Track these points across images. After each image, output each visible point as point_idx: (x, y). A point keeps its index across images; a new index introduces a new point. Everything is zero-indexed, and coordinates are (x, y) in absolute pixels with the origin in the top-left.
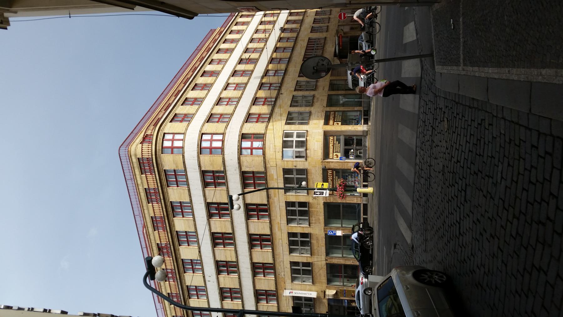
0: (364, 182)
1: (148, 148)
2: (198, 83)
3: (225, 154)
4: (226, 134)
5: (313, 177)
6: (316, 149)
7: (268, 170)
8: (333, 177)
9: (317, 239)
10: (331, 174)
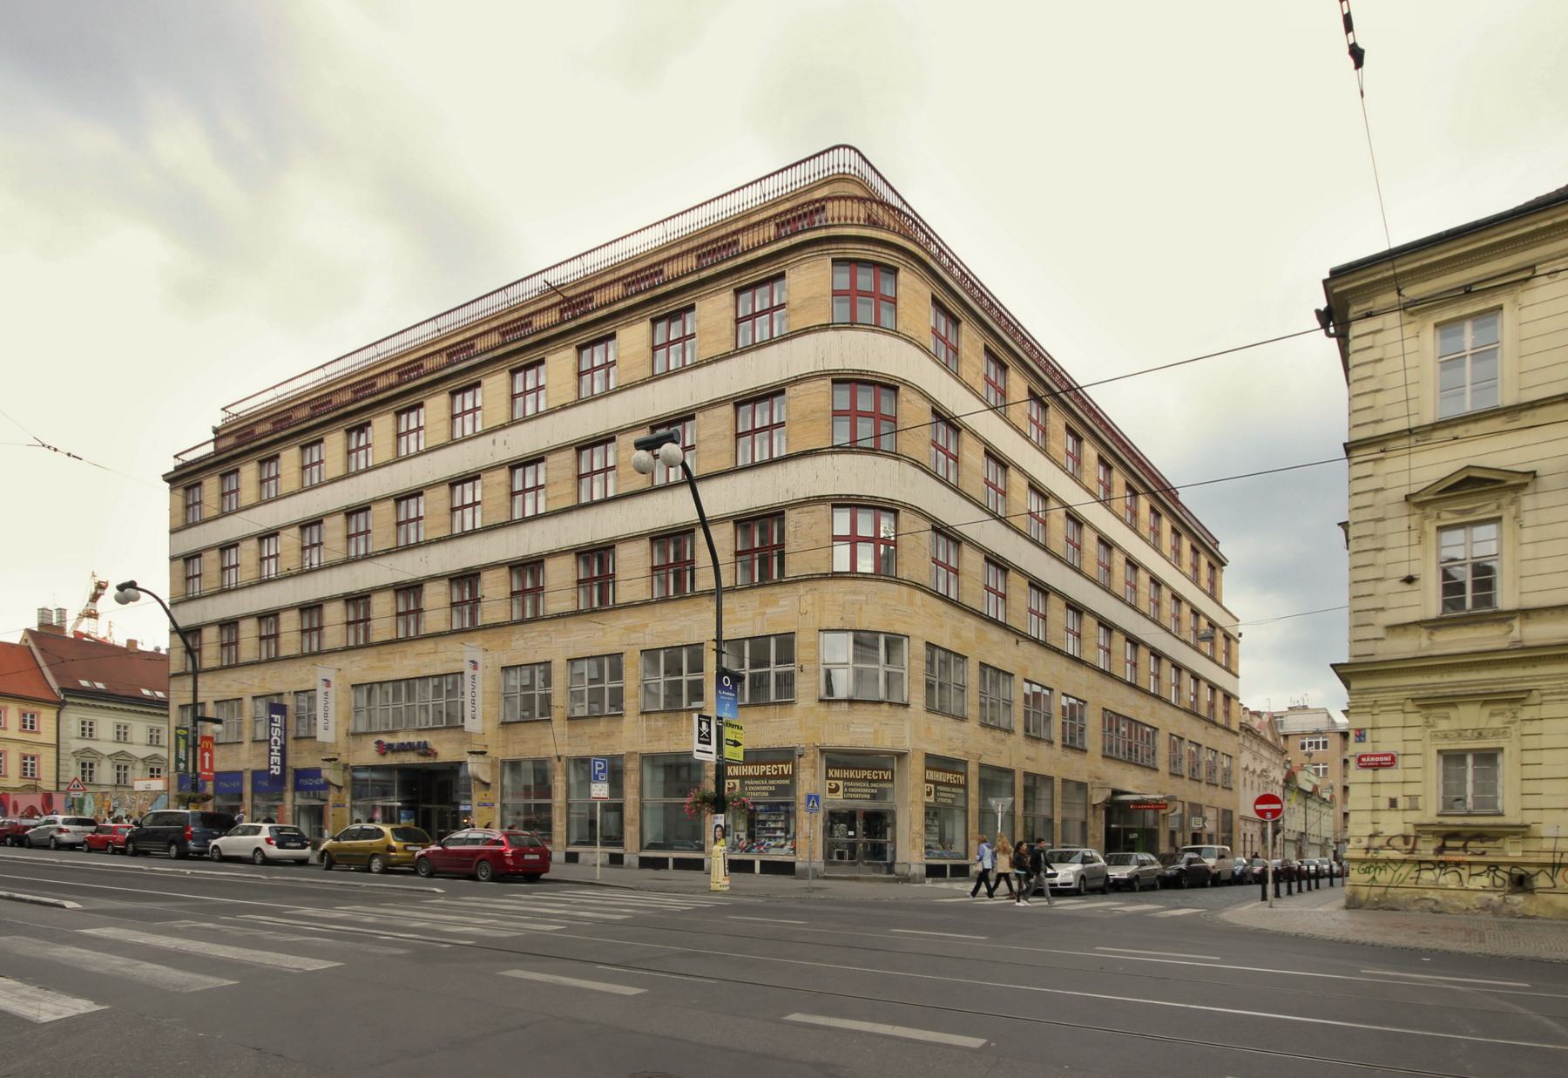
0: (762, 863)
3: (834, 456)
6: (851, 730)
7: (789, 588)
8: (772, 777)
9: (609, 735)
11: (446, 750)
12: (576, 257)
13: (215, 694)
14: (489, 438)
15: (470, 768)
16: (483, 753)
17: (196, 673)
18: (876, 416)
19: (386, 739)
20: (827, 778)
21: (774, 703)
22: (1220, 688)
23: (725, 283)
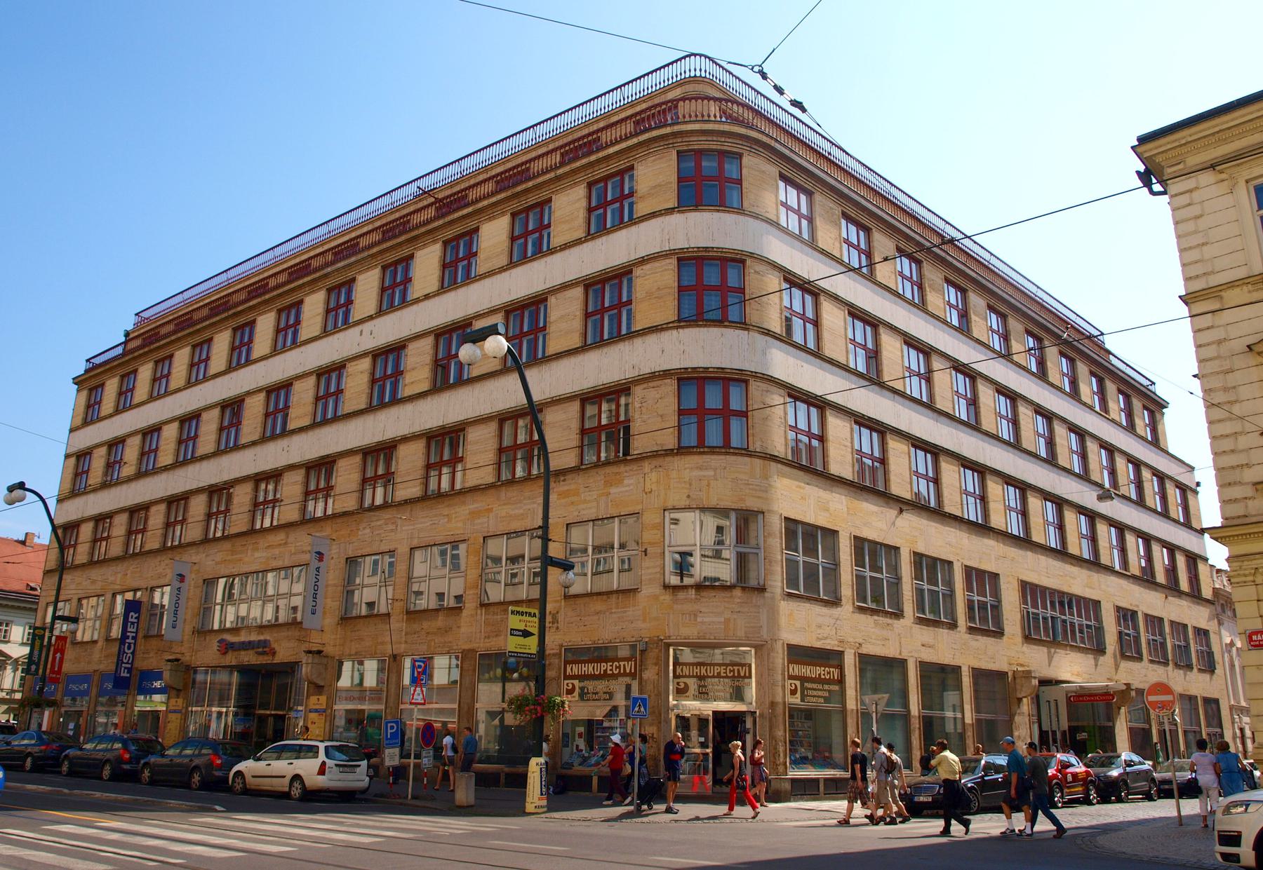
3: (681, 330)
4: (746, 332)
6: (699, 619)
9: (447, 630)
10: (622, 671)
13: (80, 592)
14: (357, 329)
16: (319, 652)
22: (1179, 548)
23: (580, 177)
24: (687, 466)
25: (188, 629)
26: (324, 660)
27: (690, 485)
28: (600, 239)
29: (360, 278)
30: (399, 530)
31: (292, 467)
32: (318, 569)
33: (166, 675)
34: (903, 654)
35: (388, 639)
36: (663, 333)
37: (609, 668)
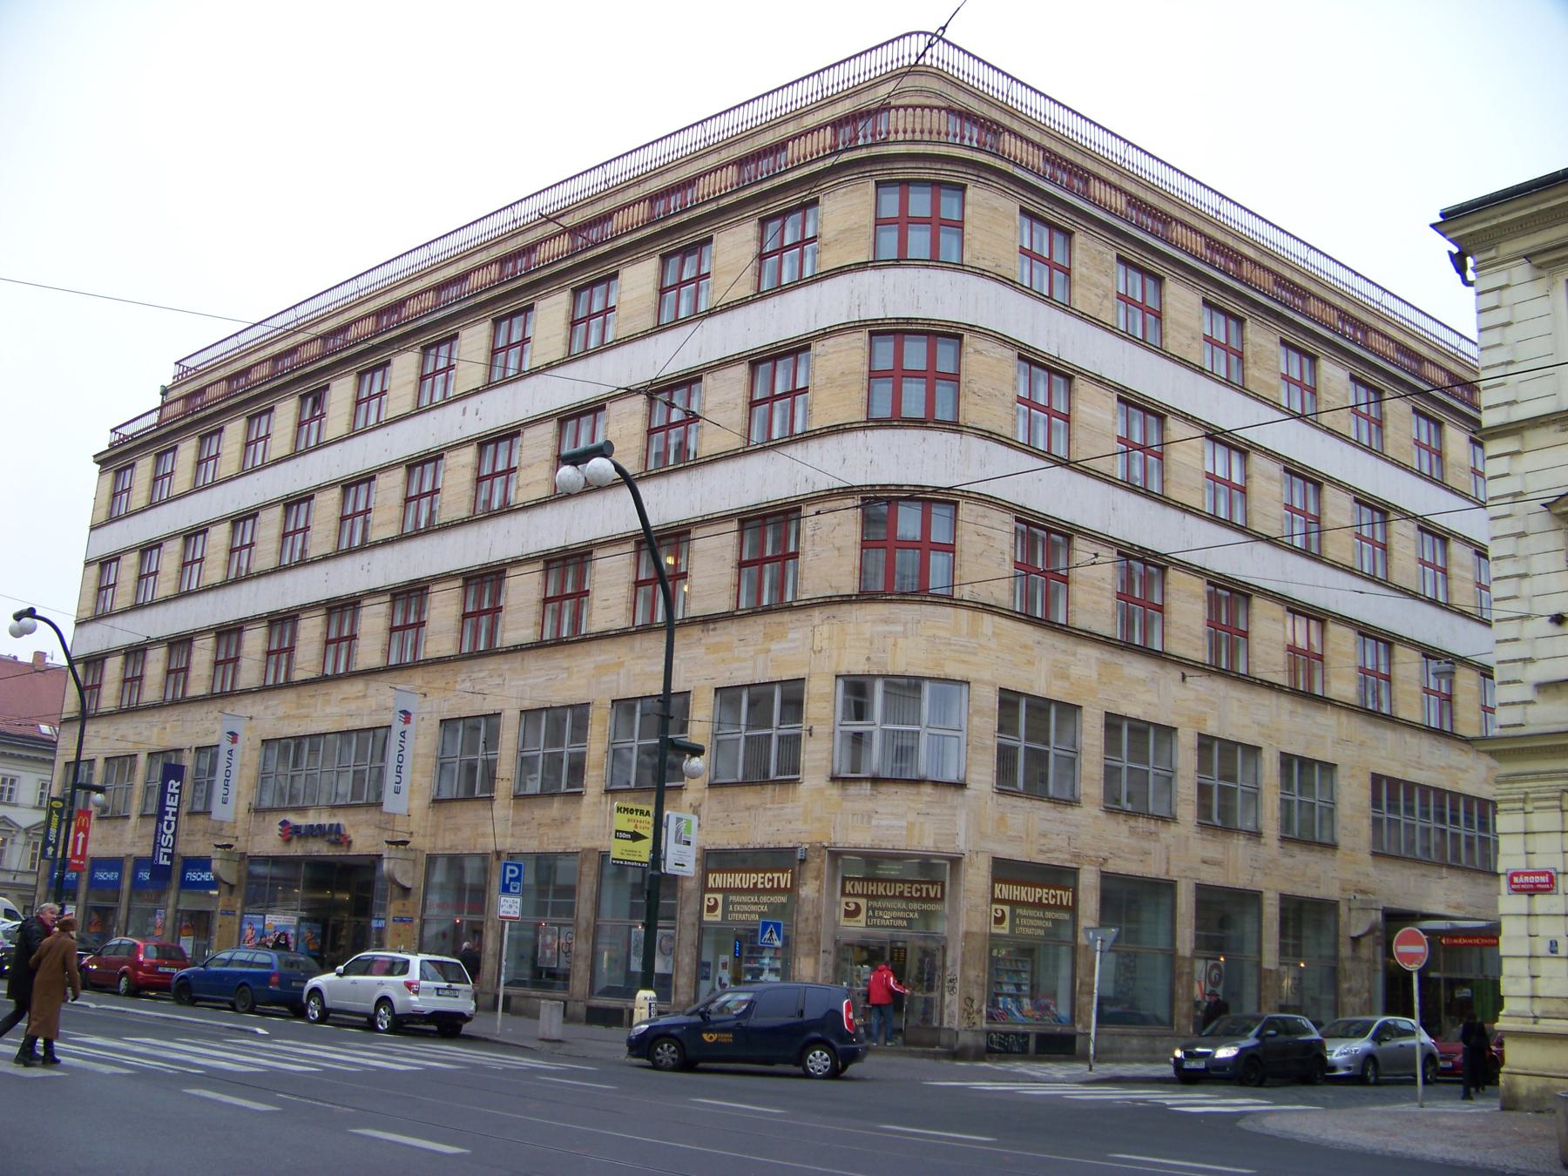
1: (935, 132)
2: (1249, 330)
3: (868, 432)
4: (958, 436)
5: (770, 809)
6: (874, 822)
8: (765, 891)
9: (564, 822)
11: (363, 838)
12: (598, 167)
14: (458, 406)
15: (386, 866)
16: (405, 843)
17: (84, 716)
18: (931, 376)
19: (294, 819)
20: (844, 894)
21: (774, 782)
24: (868, 618)
25: (243, 806)
26: (412, 855)
27: (871, 644)
28: (772, 299)
29: (464, 334)
30: (506, 686)
31: (373, 593)
32: (403, 734)
33: (215, 865)
34: (1171, 873)
35: (490, 830)
36: (845, 435)
37: (760, 880)
